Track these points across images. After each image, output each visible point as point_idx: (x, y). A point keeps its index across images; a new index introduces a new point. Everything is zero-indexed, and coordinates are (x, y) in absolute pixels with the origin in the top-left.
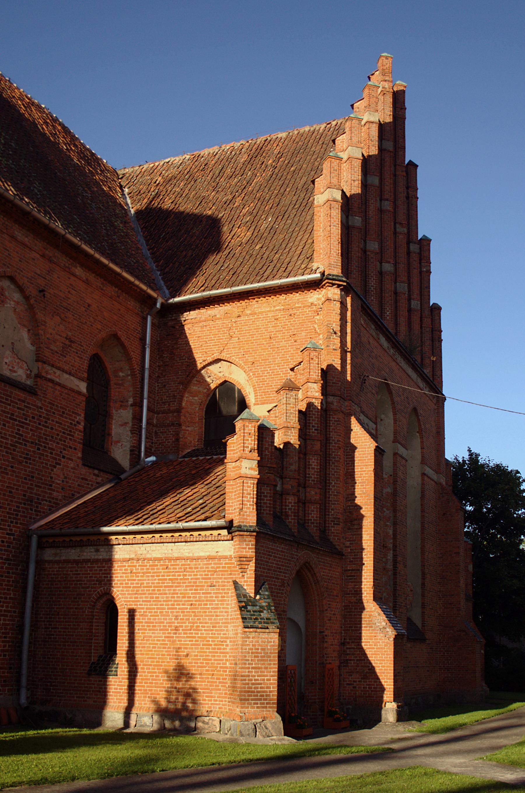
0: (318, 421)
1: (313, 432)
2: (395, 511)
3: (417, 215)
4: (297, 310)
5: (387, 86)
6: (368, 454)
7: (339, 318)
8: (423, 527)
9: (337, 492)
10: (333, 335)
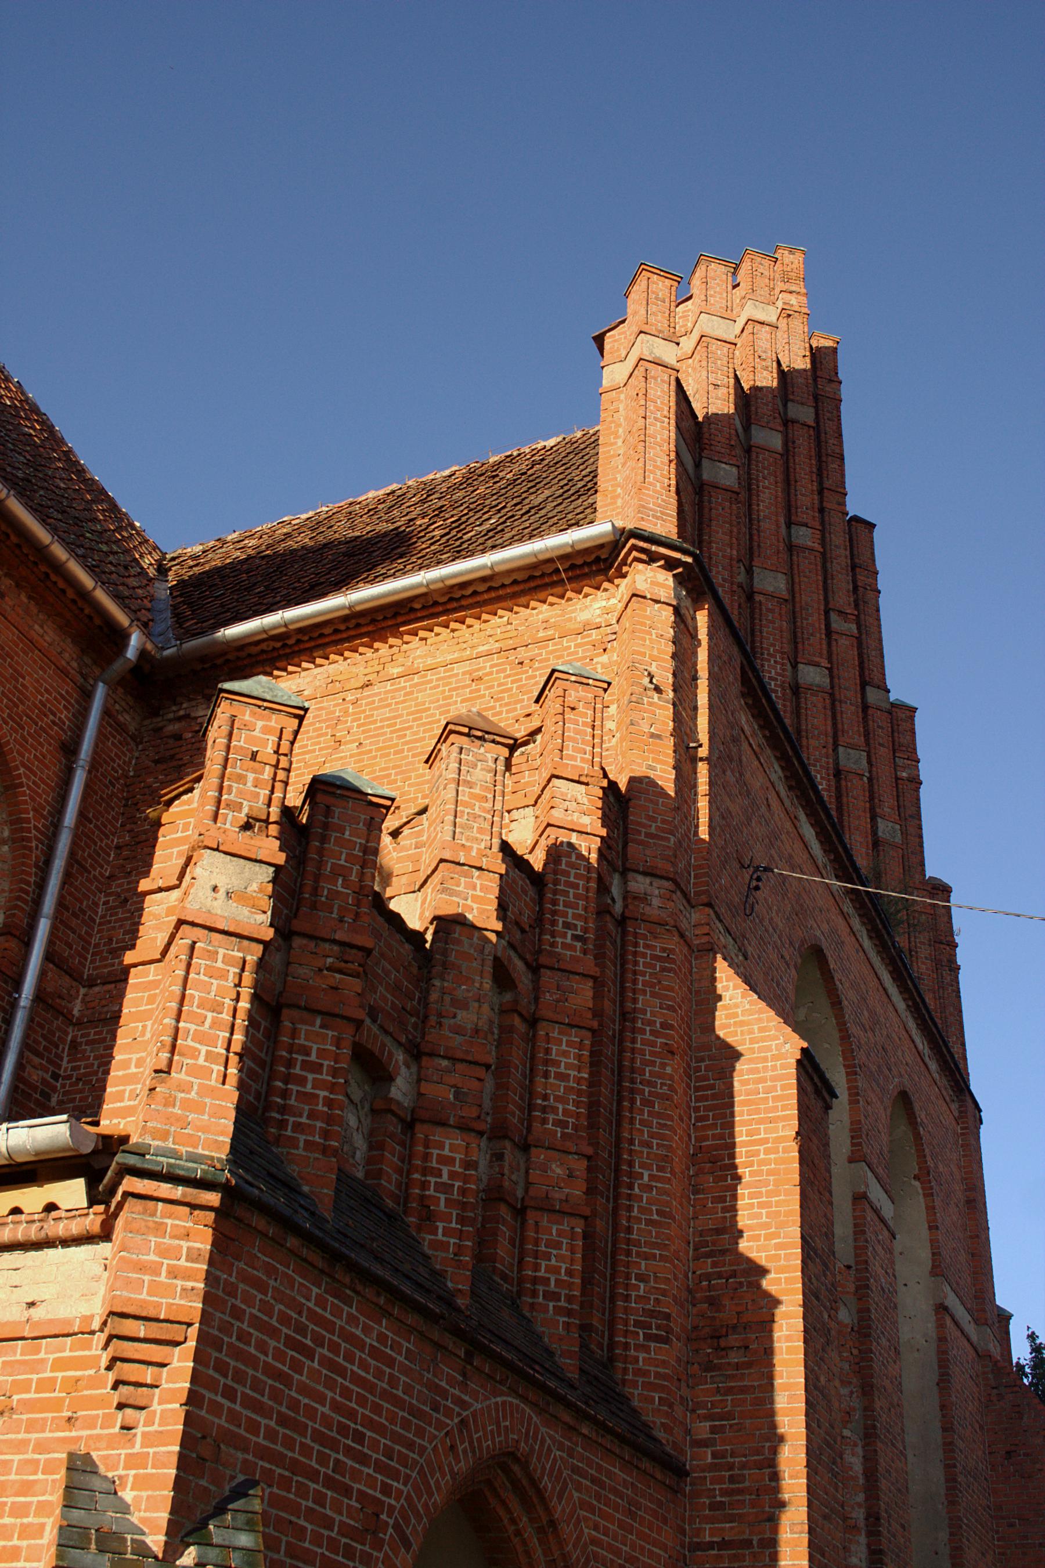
0: (585, 909)
1: (565, 946)
2: (867, 1389)
3: (879, 626)
4: (539, 648)
5: (794, 302)
6: (774, 1079)
7: (670, 649)
8: (951, 1480)
9: (658, 1212)
10: (649, 693)
